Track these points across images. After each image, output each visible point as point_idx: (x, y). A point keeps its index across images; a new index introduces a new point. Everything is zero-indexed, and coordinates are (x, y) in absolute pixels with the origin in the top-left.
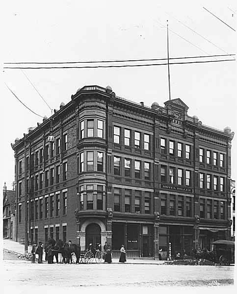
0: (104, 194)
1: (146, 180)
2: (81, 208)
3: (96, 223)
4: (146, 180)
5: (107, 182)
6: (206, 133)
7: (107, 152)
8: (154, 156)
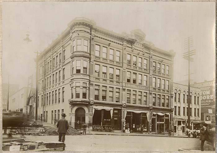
0: (88, 88)
1: (110, 79)
2: (72, 97)
3: (83, 107)
4: (110, 79)
5: (90, 81)
6: (147, 48)
7: (90, 61)
8: (150, 72)
